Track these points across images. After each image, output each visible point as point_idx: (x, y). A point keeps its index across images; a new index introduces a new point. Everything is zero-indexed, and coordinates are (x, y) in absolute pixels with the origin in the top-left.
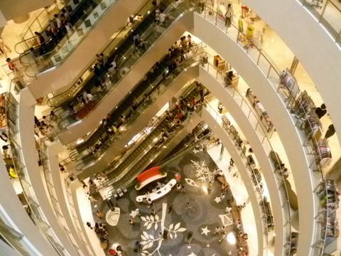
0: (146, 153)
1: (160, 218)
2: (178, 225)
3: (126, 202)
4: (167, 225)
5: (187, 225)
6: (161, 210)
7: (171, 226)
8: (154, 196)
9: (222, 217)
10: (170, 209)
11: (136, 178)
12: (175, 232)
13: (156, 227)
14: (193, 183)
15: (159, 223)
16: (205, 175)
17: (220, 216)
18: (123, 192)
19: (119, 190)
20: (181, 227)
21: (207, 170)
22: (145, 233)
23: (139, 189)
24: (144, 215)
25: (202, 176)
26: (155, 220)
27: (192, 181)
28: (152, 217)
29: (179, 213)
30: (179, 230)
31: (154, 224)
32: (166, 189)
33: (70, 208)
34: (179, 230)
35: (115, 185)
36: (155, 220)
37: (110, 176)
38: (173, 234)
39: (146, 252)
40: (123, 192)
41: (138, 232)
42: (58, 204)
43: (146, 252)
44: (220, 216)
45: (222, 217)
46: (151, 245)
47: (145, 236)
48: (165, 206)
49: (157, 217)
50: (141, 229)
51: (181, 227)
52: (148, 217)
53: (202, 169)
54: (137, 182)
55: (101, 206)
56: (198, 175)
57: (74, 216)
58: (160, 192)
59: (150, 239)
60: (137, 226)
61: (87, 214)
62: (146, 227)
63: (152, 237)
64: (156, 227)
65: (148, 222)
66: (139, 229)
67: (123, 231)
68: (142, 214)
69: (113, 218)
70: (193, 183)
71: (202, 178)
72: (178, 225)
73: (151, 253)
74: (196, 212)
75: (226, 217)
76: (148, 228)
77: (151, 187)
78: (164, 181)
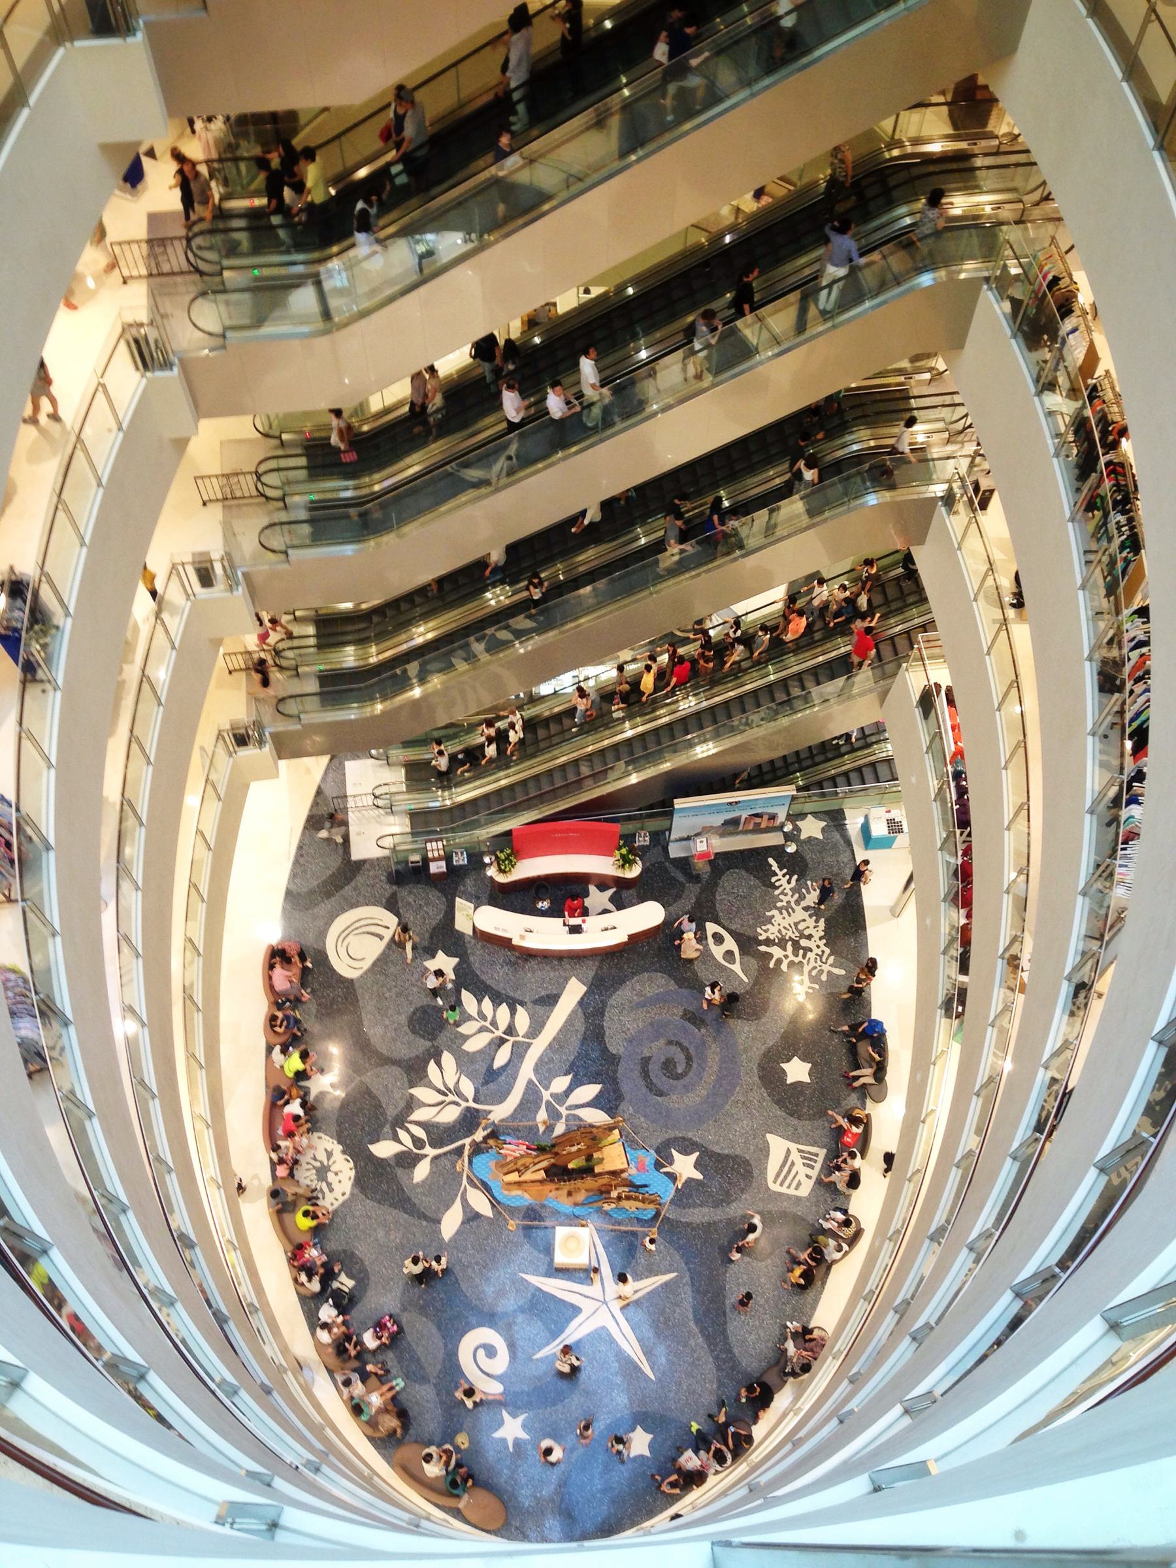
0: (629, 734)
1: (535, 1030)
2: (590, 1091)
3: (424, 905)
4: (545, 1070)
5: (627, 1108)
6: (551, 1000)
7: (561, 1083)
8: (543, 933)
9: (778, 1146)
10: (592, 1009)
11: (509, 833)
12: (562, 1110)
13: (502, 1057)
14: (729, 954)
15: (519, 1052)
16: (796, 946)
17: (770, 1137)
18: (448, 858)
19: (435, 848)
20: (594, 1103)
21: (816, 929)
22: (447, 1059)
23: (501, 879)
24: (481, 990)
25: (782, 943)
26: (511, 1030)
27: (730, 944)
28: (504, 1009)
29: (615, 1045)
30: (582, 1113)
31: (502, 1041)
32: (611, 927)
33: (187, 848)
34: (582, 1113)
35: (422, 821)
36: (511, 1030)
37: (420, 775)
38: (554, 1115)
39: (420, 1133)
40: (448, 858)
41: (423, 1044)
42: (155, 1107)
43: (420, 1133)
44: (770, 1137)
45: (778, 1146)
46: (450, 1115)
47: (445, 1071)
48: (574, 991)
49: (523, 1020)
50: (442, 1038)
51: (594, 1103)
52: (487, 1002)
53: (800, 914)
54: (510, 847)
55: (329, 871)
56: (770, 932)
57: (193, 886)
58: (576, 930)
59: (459, 1094)
60: (432, 1024)
61: (258, 917)
62: (466, 1038)
63: (468, 1088)
64: (502, 1057)
65: (480, 1022)
66: (432, 1036)
67: (368, 1005)
68: (467, 978)
69: (357, 941)
70: (729, 954)
71: (776, 952)
72: (590, 1091)
73: (433, 1146)
74: (678, 1077)
75: (795, 1156)
76: (472, 1046)
77: (563, 896)
78: (624, 894)
